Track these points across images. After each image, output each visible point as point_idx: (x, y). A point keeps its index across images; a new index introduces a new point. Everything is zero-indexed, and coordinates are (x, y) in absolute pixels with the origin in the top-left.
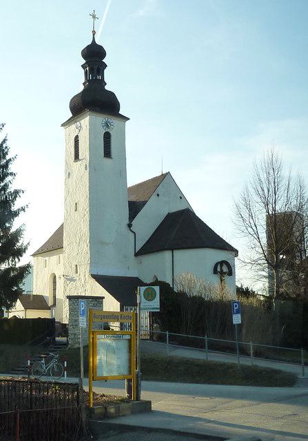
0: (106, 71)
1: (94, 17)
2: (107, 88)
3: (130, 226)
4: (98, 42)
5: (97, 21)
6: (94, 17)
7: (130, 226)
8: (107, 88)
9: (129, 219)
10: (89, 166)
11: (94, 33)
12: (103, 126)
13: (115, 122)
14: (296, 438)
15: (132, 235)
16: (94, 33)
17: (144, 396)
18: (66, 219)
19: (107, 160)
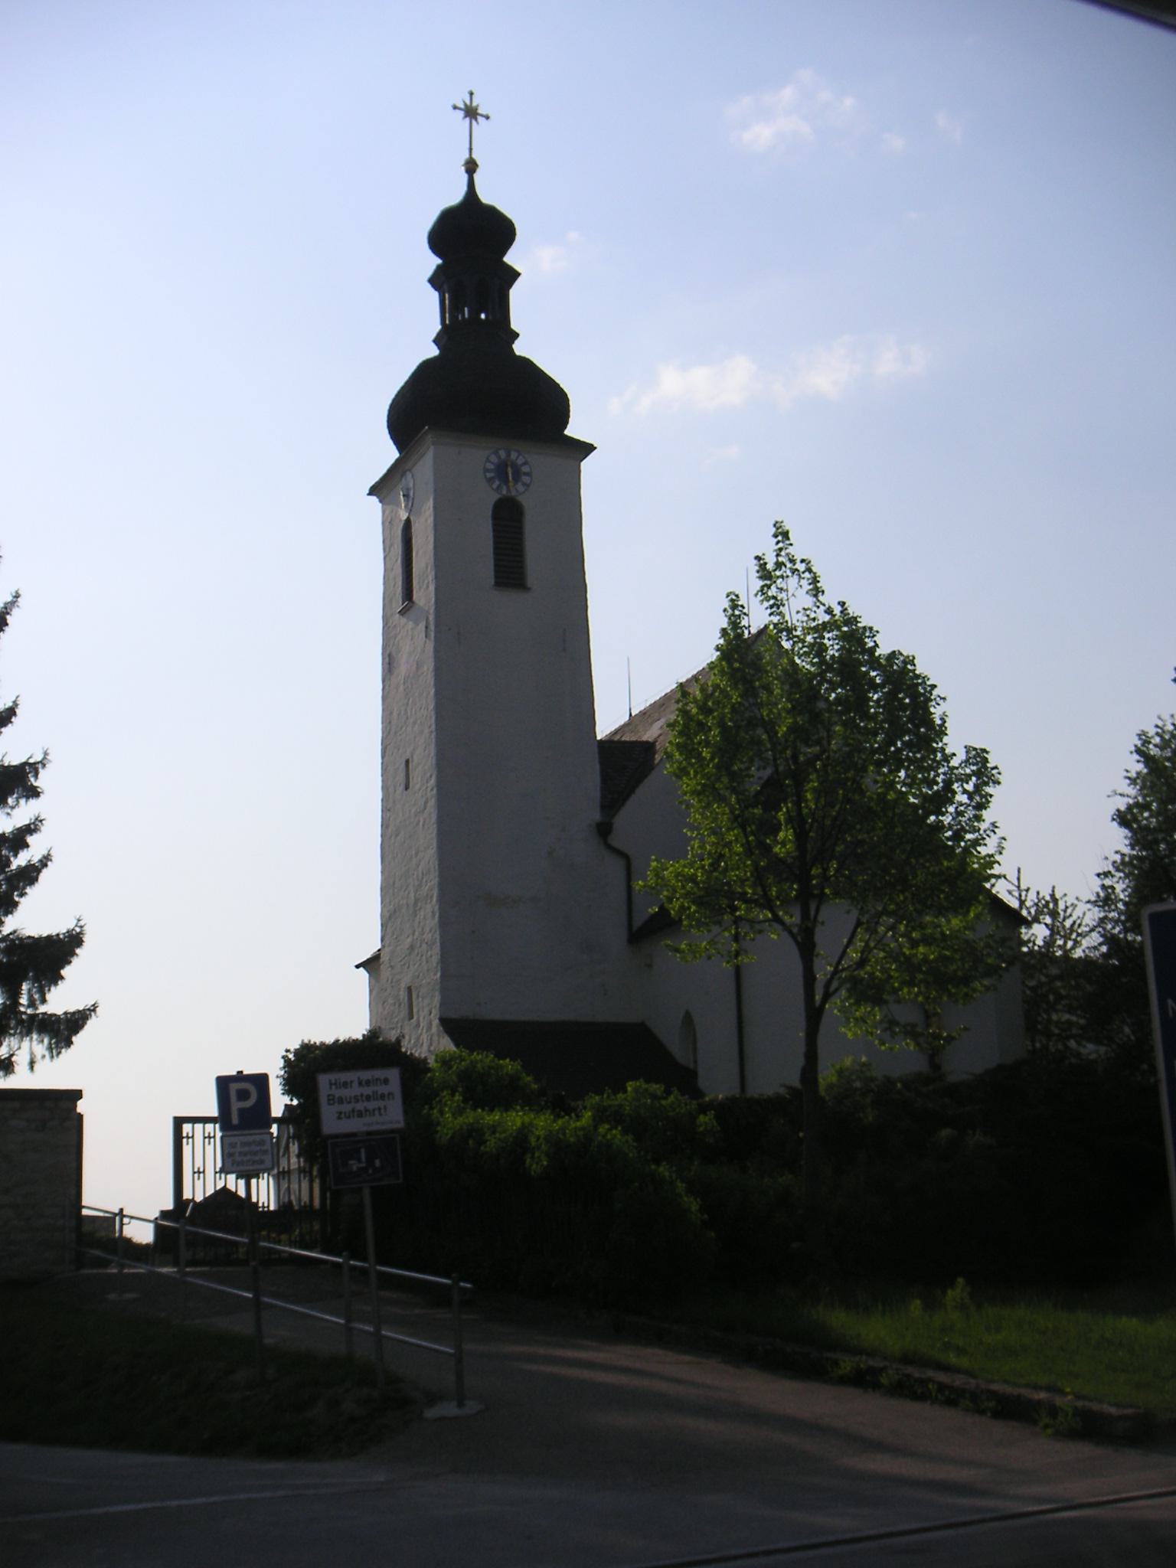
0: (516, 293)
1: (471, 113)
2: (520, 348)
3: (604, 830)
4: (486, 197)
5: (481, 127)
6: (471, 113)
7: (604, 830)
8: (520, 348)
9: (603, 807)
10: (437, 626)
11: (471, 167)
12: (490, 480)
13: (537, 461)
14: (230, 1269)
15: (614, 868)
16: (471, 167)
17: (831, 662)
18: (383, 946)
19: (509, 601)
